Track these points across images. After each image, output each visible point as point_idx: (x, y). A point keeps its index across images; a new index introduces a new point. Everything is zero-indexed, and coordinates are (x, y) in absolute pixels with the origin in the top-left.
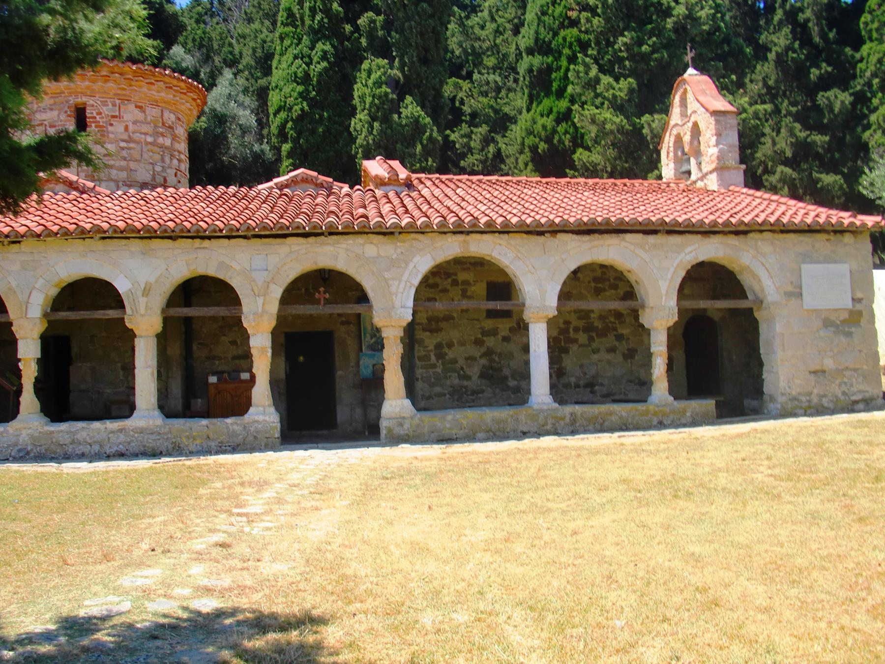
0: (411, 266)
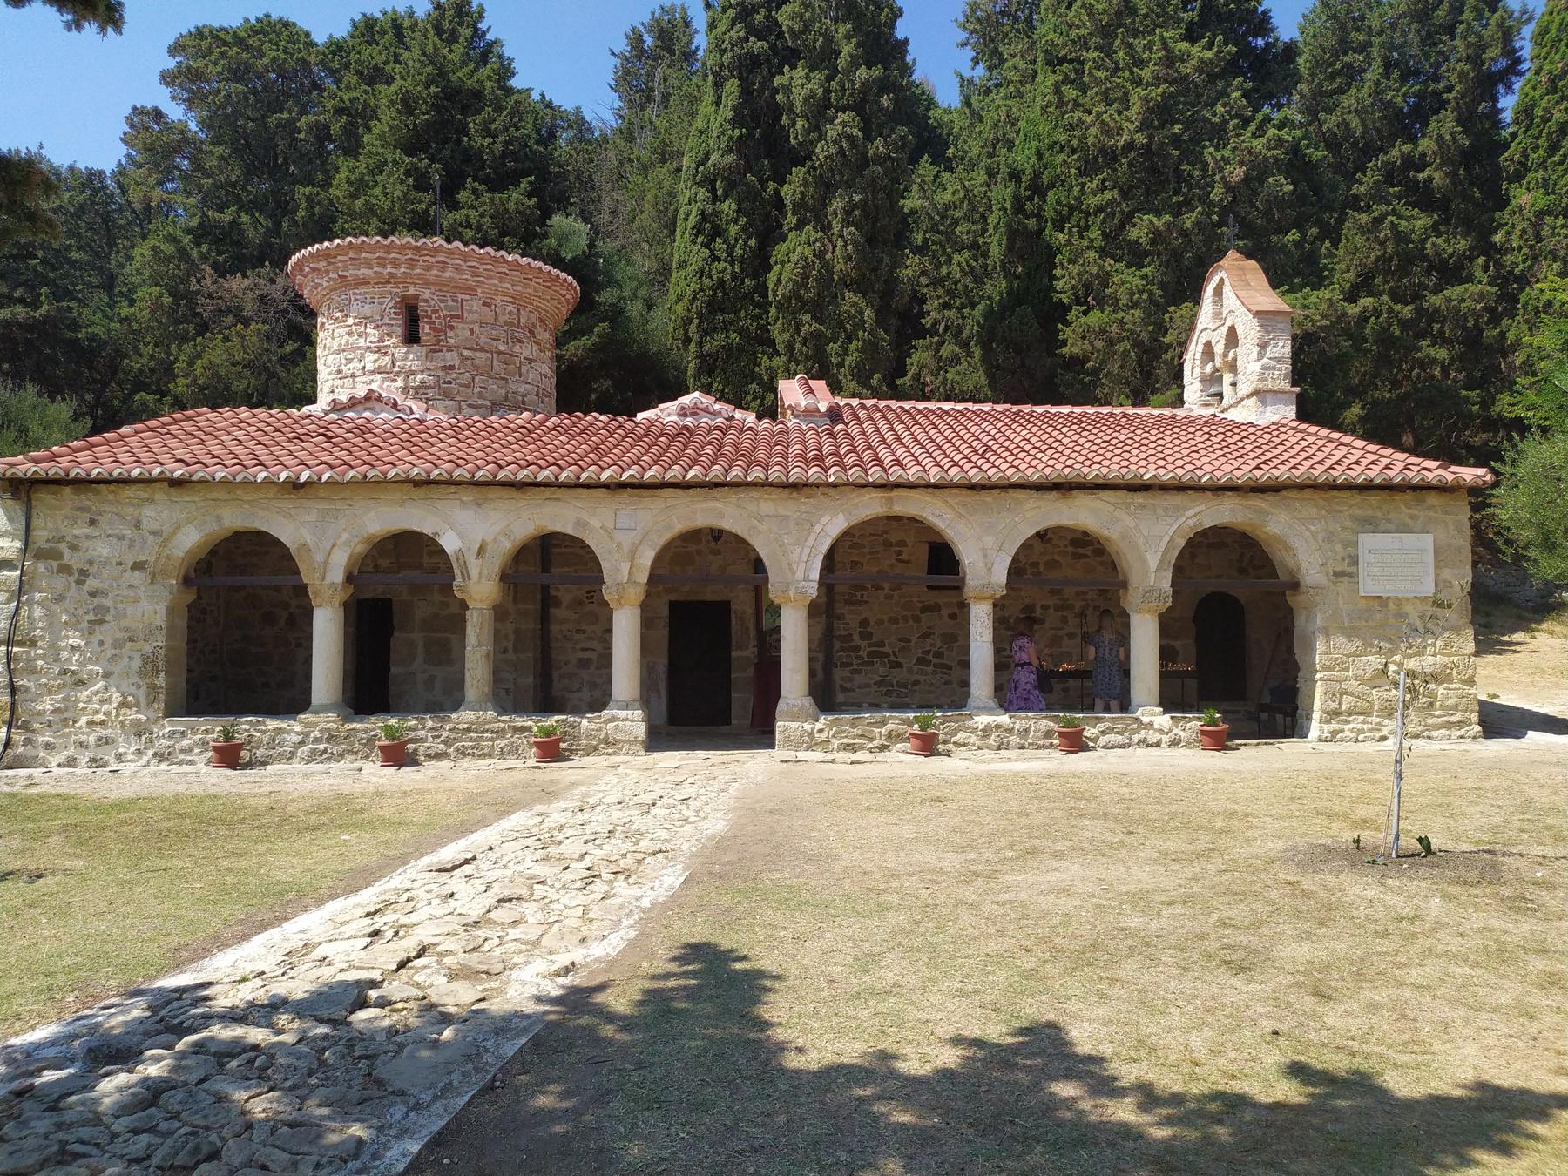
0: (818, 528)
